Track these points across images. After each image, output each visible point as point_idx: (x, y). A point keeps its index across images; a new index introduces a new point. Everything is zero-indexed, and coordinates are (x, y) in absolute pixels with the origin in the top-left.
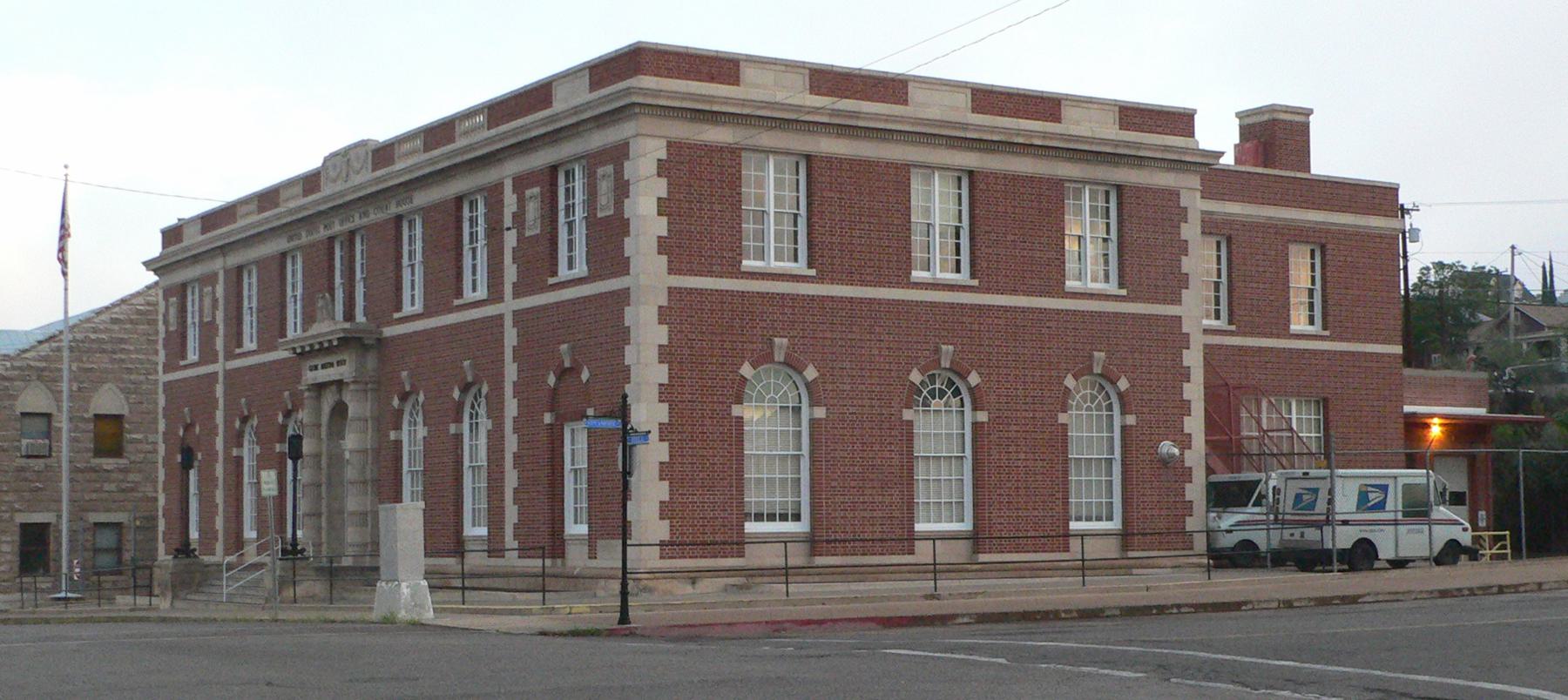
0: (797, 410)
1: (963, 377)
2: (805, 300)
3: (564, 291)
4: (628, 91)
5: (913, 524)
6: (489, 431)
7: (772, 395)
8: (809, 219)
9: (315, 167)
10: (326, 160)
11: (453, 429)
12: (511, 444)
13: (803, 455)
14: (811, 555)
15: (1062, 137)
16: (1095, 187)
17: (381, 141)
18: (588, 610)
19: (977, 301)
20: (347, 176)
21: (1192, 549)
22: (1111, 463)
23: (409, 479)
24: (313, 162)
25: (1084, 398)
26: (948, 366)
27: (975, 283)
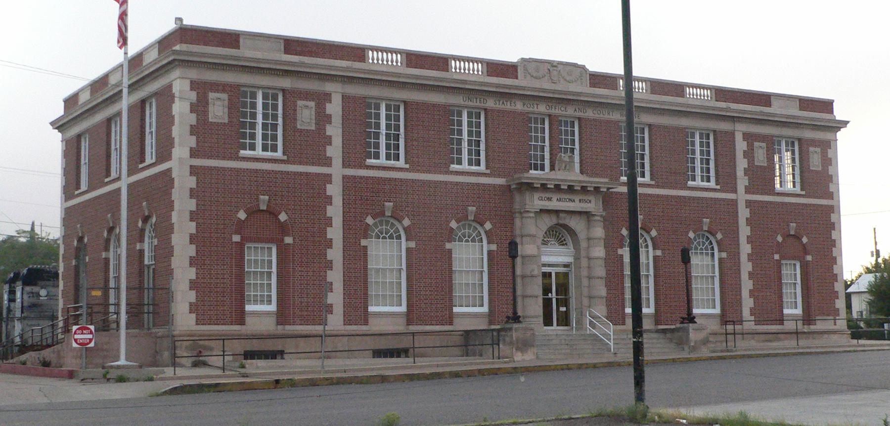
0: (713, 255)
1: (714, 235)
2: (219, 170)
5: (368, 307)
7: (384, 235)
8: (580, 150)
12: (746, 267)
13: (715, 276)
14: (407, 325)
15: (517, 88)
16: (266, 91)
19: (819, 200)
22: (714, 278)
24: (512, 57)
25: (699, 243)
26: (707, 230)
27: (718, 187)
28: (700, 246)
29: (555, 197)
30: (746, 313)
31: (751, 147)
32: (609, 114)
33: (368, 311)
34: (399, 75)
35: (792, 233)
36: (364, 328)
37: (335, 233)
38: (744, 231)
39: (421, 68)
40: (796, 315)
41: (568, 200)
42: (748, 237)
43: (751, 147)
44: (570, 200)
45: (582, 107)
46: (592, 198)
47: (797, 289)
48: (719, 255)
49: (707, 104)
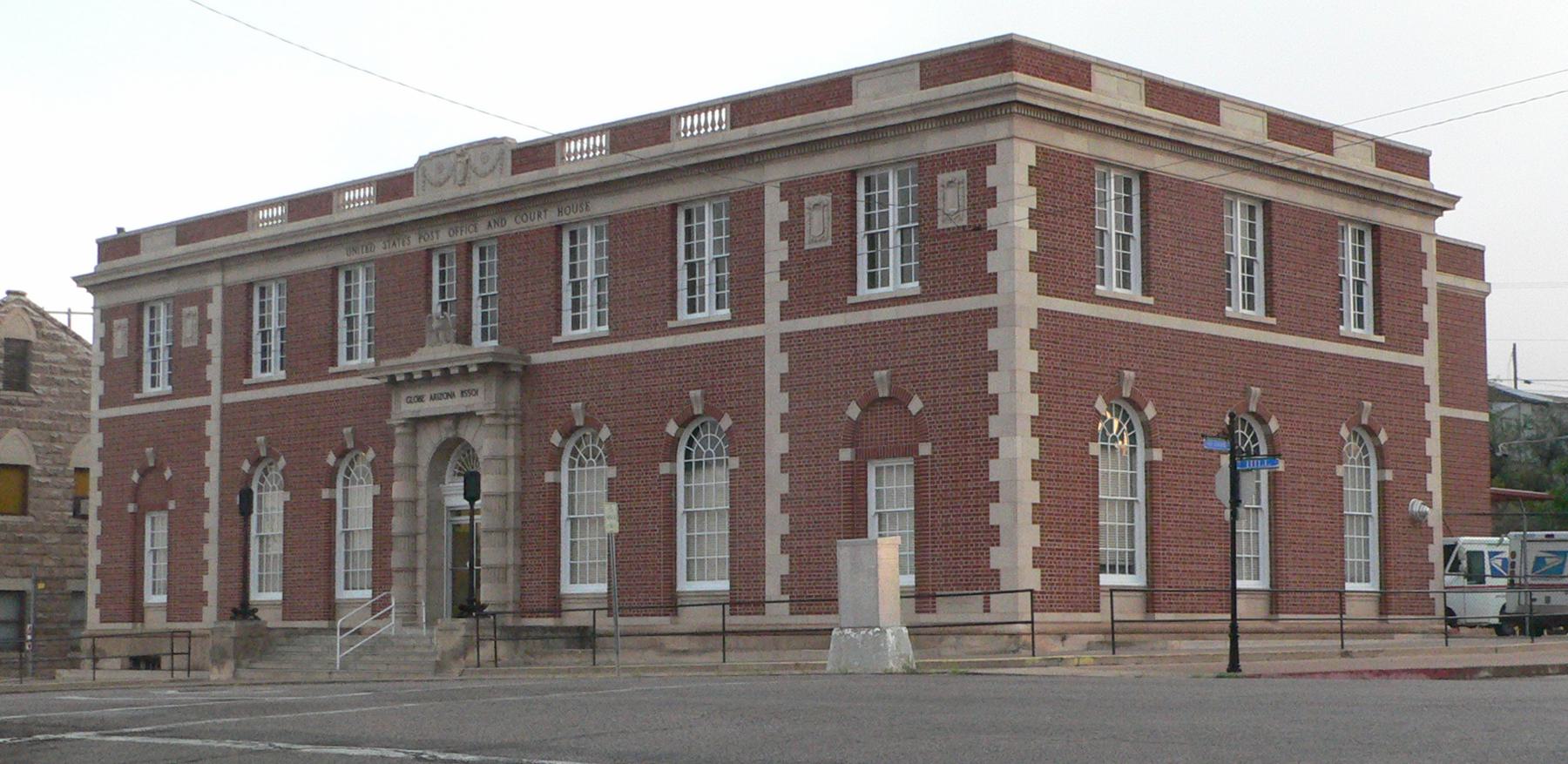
3: (874, 311)
4: (1012, 87)
6: (375, 496)
9: (404, 167)
10: (422, 160)
11: (325, 494)
12: (777, 483)
15: (420, 208)
16: (716, 202)
17: (518, 141)
18: (1092, 660)
20: (465, 178)
21: (1434, 614)
23: (569, 528)
24: (403, 160)
29: (427, 392)
30: (772, 589)
31: (797, 212)
32: (539, 216)
35: (884, 392)
38: (776, 403)
39: (955, 82)
40: (596, 597)
42: (783, 416)
43: (797, 212)
46: (478, 385)
47: (1136, 519)
48: (675, 468)
49: (719, 139)
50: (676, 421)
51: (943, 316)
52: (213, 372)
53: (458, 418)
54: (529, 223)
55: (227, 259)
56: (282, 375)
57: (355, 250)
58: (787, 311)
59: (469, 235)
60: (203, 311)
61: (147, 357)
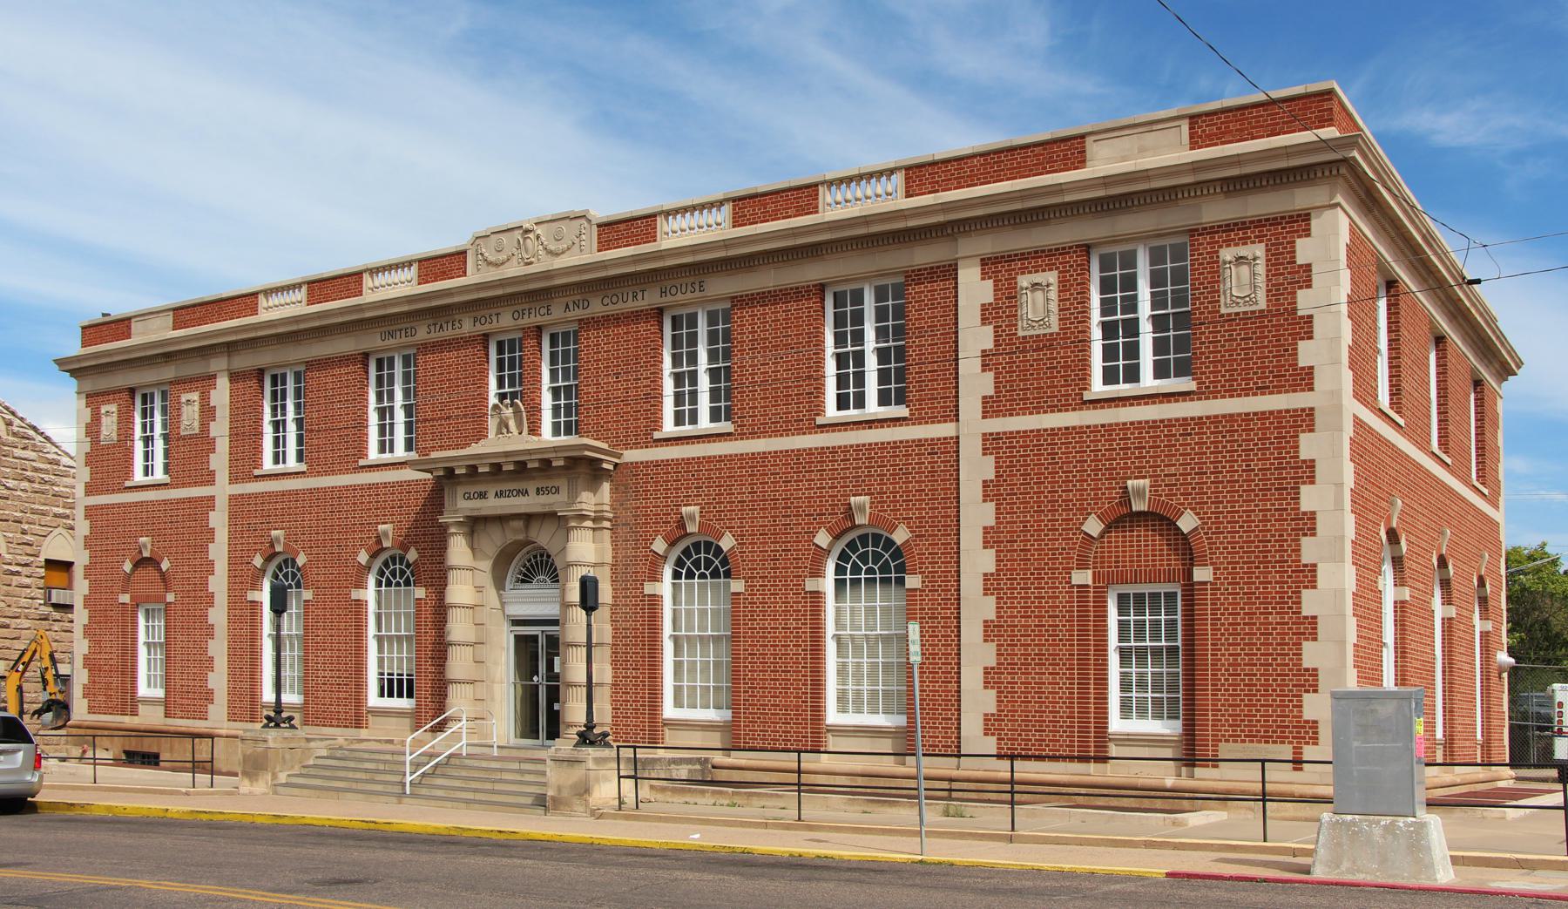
28: (395, 578)
31: (204, 427)
32: (635, 297)
33: (1106, 732)
34: (726, 244)
36: (1093, 772)
37: (219, 583)
41: (515, 493)
43: (204, 427)
44: (519, 492)
45: (578, 297)
50: (829, 530)
51: (1231, 418)
52: (220, 461)
53: (528, 518)
54: (620, 305)
55: (235, 342)
56: (166, 479)
57: (391, 334)
58: (991, 407)
59: (539, 318)
60: (205, 398)
61: (139, 448)
